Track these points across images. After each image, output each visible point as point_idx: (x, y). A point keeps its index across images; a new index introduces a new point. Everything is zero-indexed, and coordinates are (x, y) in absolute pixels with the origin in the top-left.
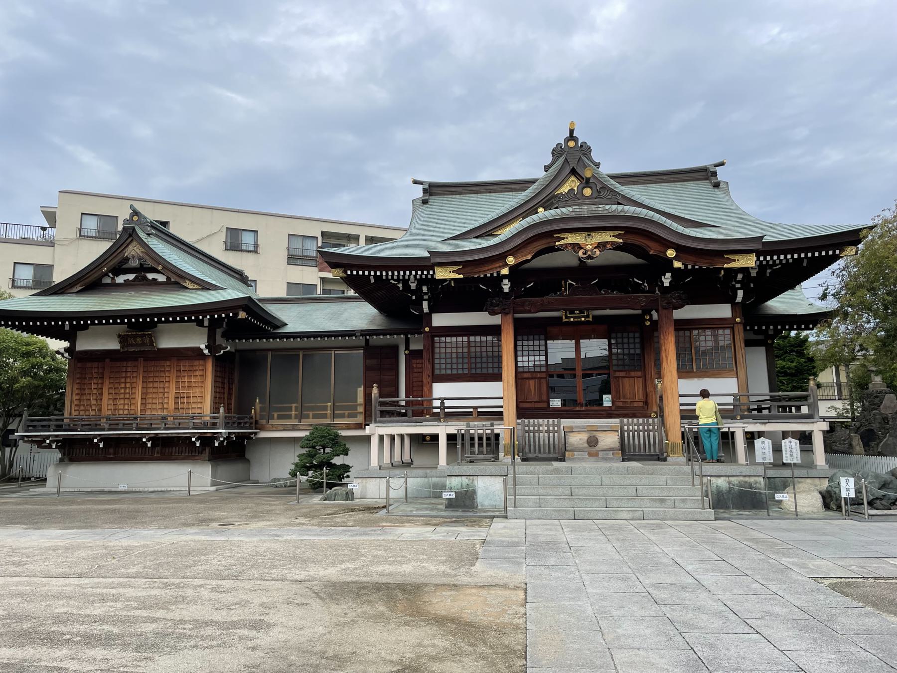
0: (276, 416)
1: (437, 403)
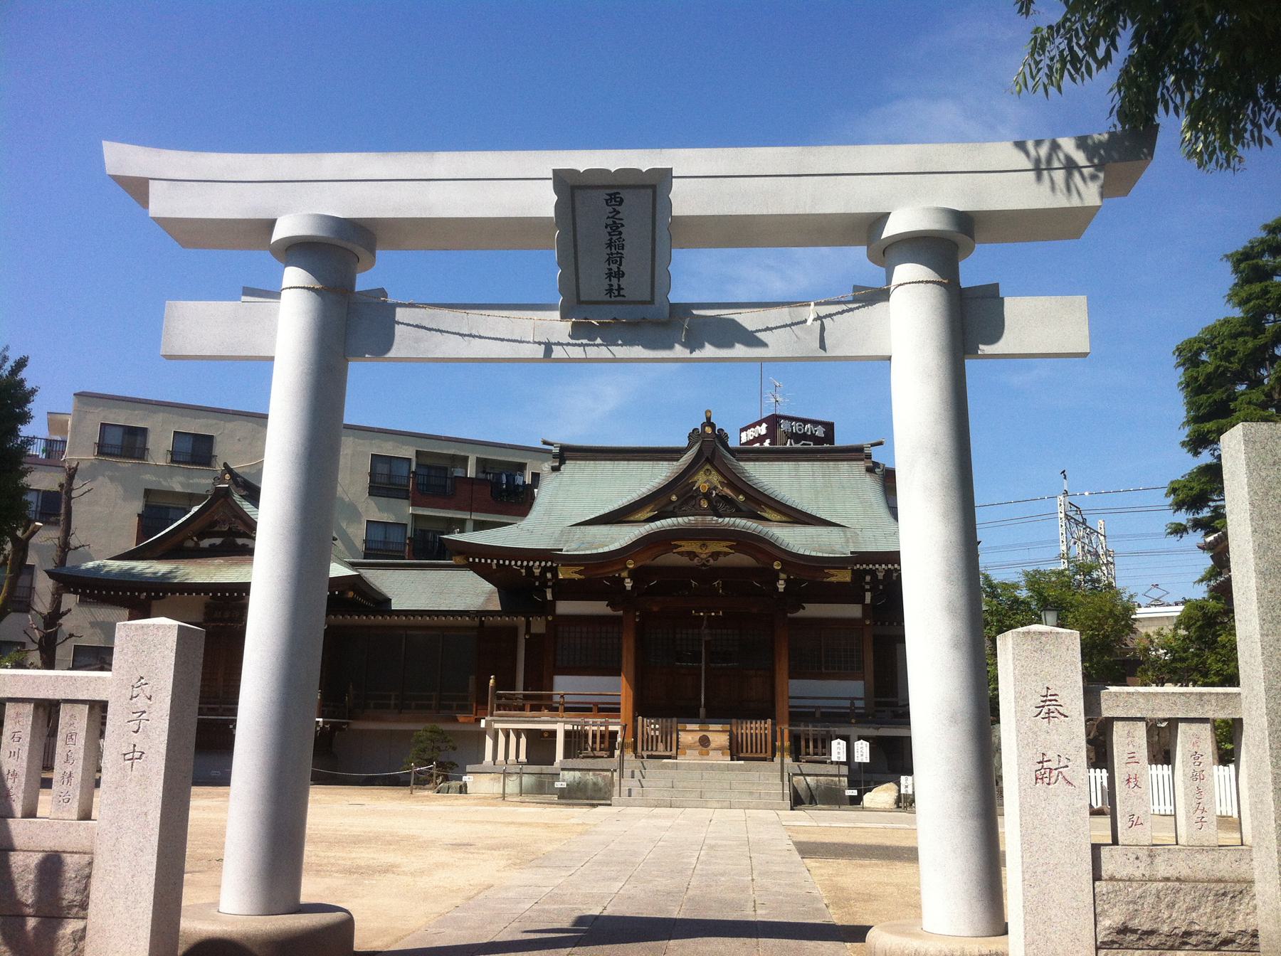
0: (372, 706)
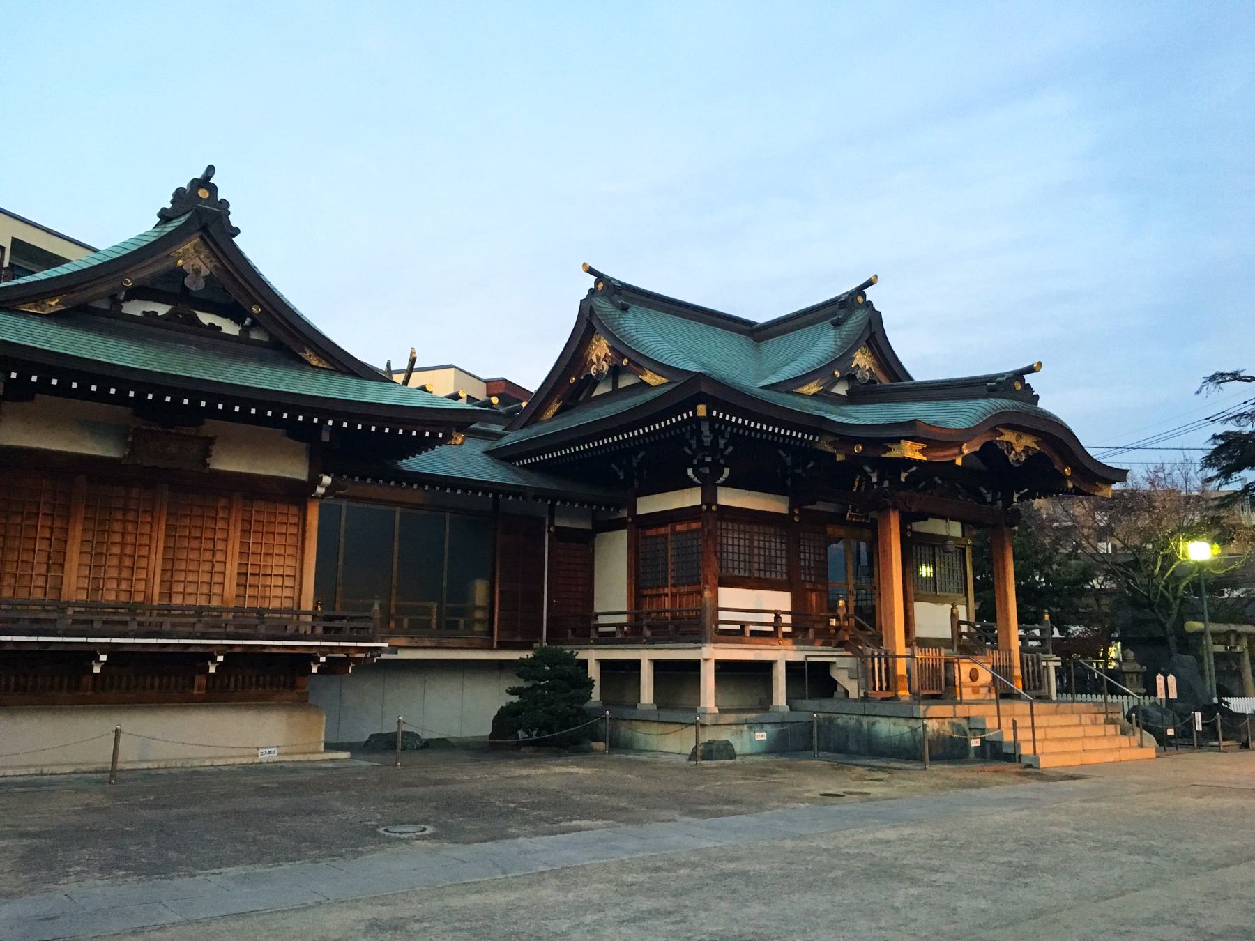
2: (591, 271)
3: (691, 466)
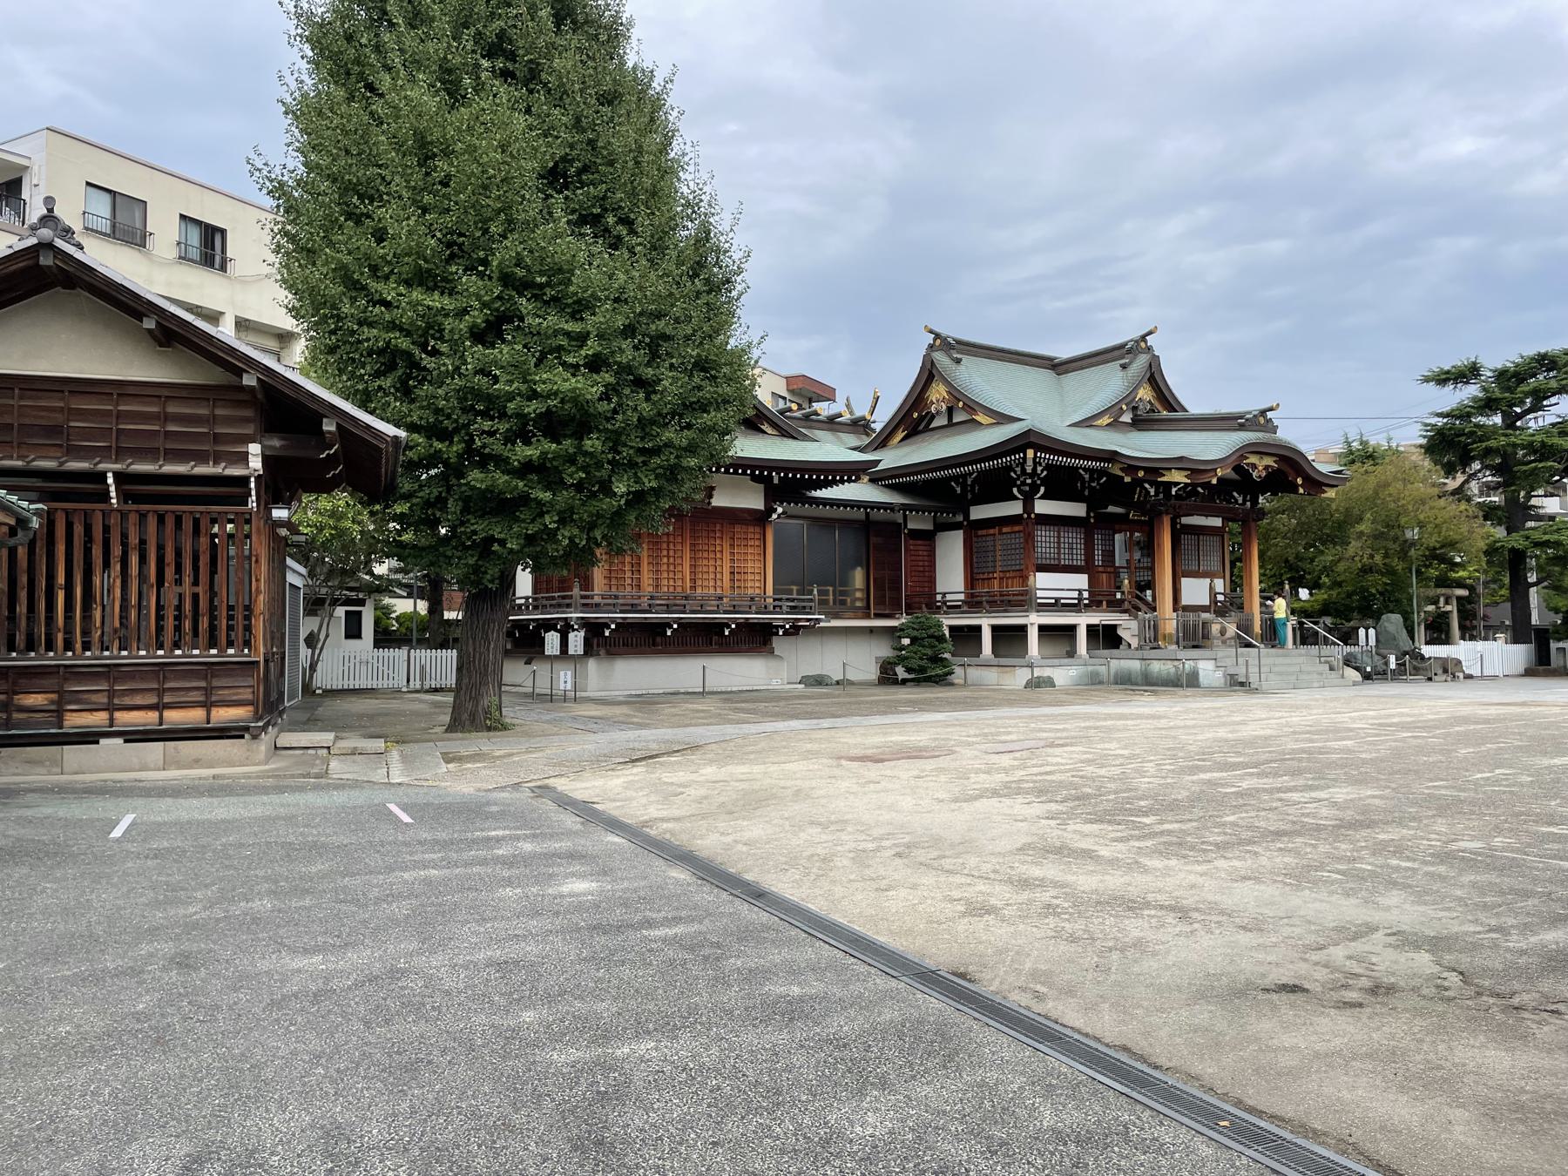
1: (939, 597)
2: (931, 332)
3: (1015, 485)
